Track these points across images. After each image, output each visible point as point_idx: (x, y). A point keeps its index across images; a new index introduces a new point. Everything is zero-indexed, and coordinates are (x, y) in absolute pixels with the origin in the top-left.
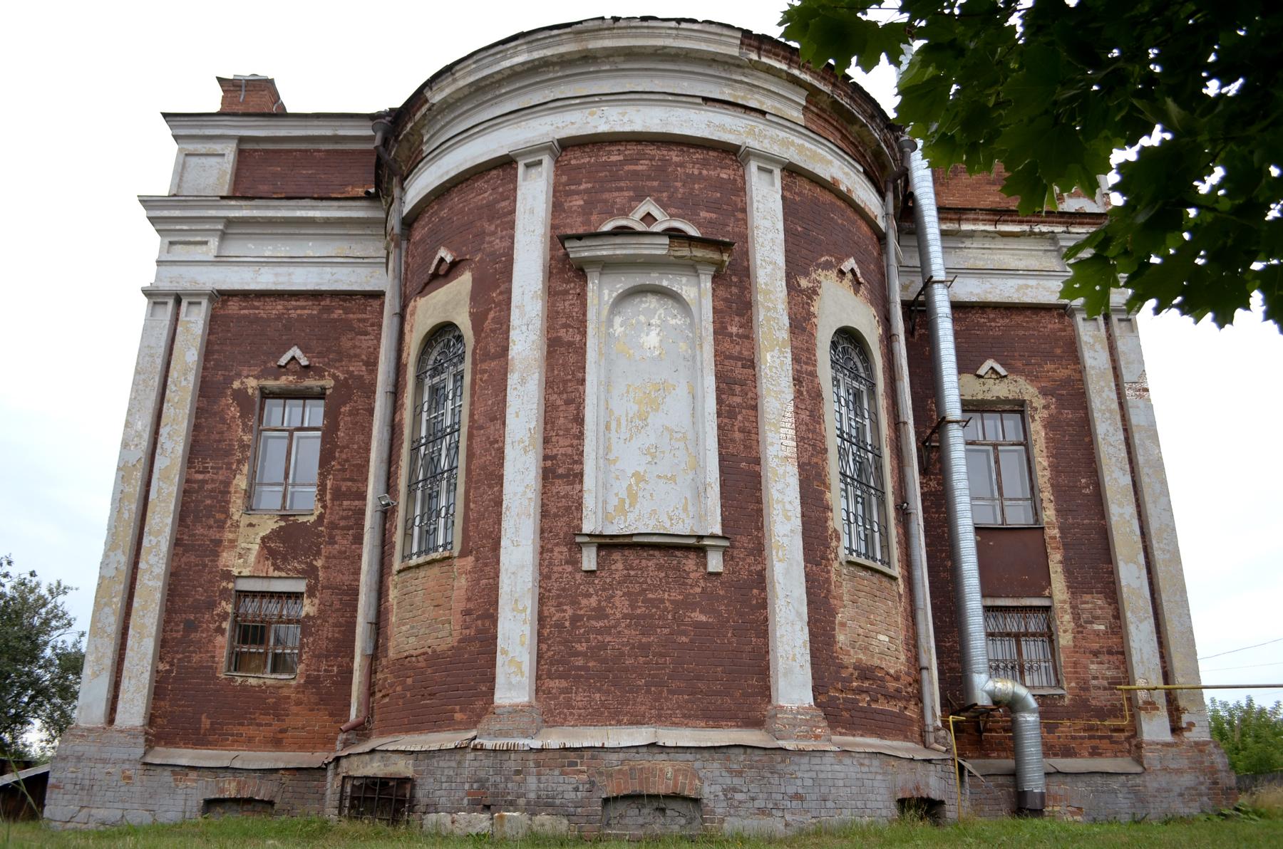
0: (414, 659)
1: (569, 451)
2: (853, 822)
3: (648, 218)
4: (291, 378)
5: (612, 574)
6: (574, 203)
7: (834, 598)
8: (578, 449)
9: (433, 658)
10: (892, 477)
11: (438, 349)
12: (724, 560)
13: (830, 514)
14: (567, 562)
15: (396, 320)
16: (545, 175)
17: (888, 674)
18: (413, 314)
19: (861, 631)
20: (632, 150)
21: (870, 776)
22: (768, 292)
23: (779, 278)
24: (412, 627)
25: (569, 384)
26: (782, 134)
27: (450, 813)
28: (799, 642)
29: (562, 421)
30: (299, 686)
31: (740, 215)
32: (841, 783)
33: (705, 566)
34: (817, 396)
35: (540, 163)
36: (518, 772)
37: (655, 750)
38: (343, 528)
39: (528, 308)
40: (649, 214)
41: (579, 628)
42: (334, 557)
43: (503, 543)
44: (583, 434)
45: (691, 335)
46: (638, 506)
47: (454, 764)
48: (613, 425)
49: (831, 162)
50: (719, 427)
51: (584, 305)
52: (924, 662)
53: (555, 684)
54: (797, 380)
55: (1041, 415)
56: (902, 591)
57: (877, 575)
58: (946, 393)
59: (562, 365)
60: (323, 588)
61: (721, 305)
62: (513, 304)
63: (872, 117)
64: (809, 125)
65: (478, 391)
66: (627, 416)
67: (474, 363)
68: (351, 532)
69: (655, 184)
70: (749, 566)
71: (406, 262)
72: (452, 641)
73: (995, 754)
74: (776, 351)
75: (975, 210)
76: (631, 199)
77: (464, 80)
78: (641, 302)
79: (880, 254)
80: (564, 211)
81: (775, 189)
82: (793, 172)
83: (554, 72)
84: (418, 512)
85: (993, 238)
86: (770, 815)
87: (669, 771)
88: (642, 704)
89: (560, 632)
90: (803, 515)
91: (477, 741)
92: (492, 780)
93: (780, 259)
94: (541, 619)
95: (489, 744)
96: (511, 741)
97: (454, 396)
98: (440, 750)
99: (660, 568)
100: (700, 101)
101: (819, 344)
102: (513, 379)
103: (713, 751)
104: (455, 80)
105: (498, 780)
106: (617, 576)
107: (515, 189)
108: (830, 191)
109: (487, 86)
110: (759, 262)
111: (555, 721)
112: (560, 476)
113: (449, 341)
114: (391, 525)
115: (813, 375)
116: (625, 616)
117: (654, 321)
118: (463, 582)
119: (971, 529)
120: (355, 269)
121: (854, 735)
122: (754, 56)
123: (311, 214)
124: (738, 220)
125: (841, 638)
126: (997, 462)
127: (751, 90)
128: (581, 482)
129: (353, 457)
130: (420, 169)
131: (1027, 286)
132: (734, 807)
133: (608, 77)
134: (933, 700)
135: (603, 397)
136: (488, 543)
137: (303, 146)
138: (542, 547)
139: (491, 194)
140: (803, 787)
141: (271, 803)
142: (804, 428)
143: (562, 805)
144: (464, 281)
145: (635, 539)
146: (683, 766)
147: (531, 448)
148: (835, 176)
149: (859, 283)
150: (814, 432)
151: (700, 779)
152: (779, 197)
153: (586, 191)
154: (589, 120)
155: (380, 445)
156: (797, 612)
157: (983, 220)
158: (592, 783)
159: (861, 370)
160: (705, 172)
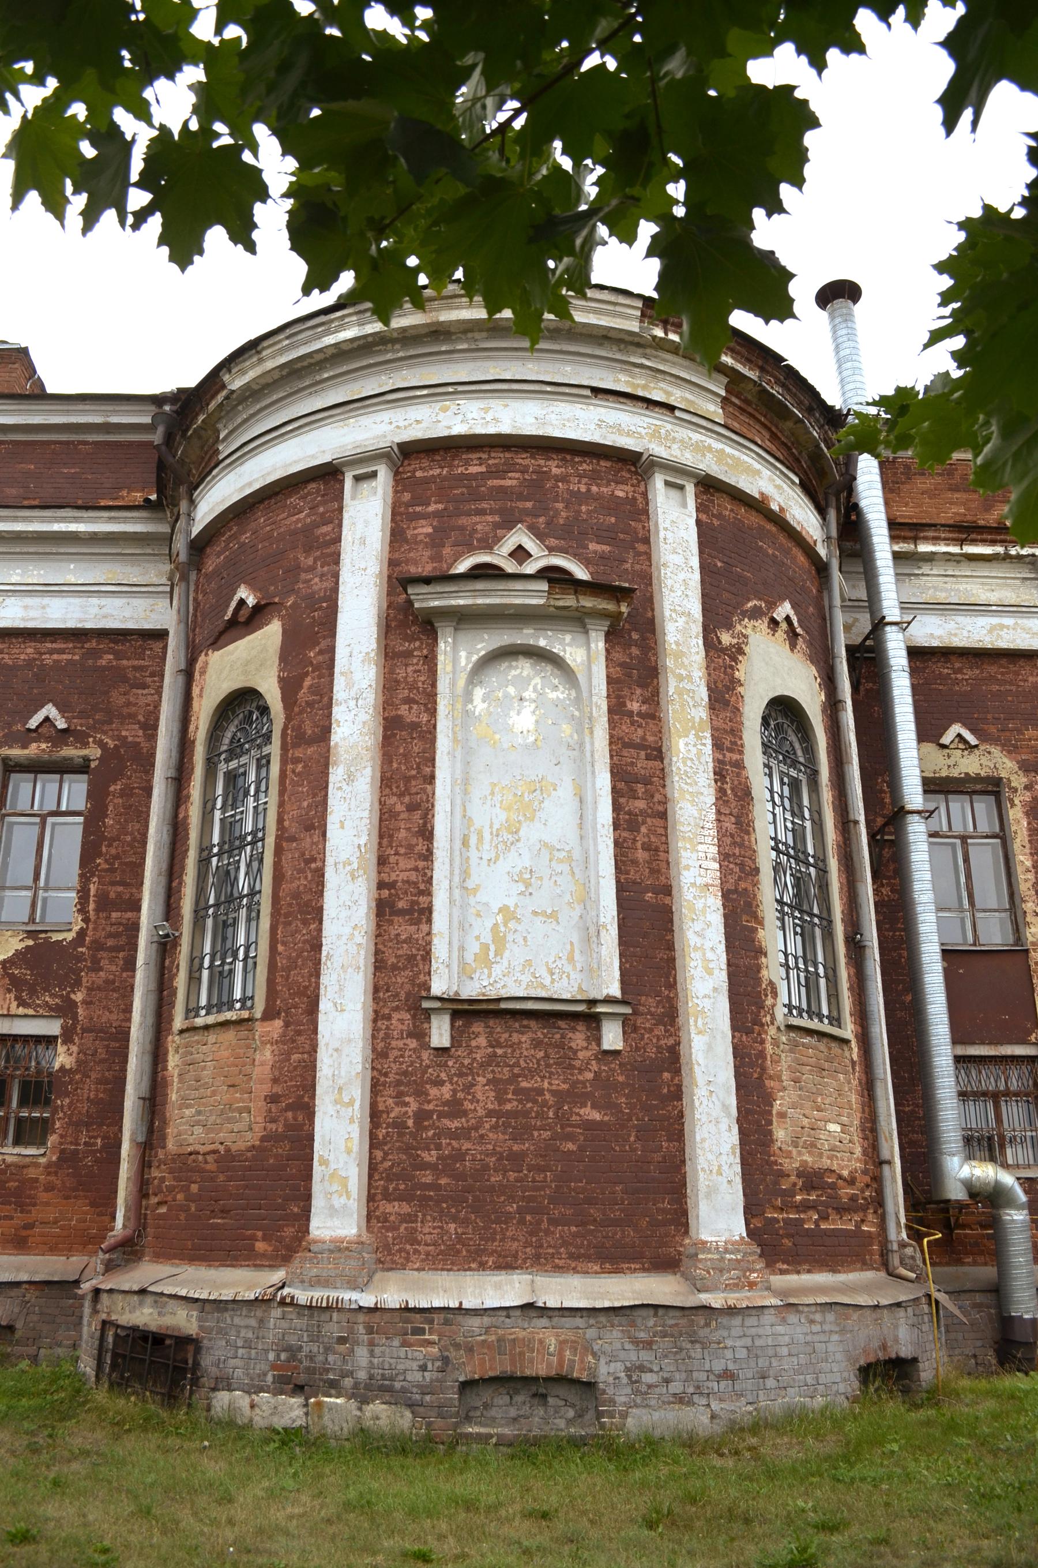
0: (200, 1158)
1: (413, 876)
2: (804, 1406)
3: (520, 554)
4: (44, 746)
5: (471, 1052)
6: (420, 530)
7: (771, 1078)
8: (425, 874)
9: (227, 1159)
10: (841, 899)
11: (236, 722)
12: (624, 1033)
13: (763, 960)
14: (410, 1035)
15: (181, 679)
16: (380, 491)
17: (840, 1177)
18: (203, 673)
19: (805, 1122)
20: (497, 458)
21: (823, 1337)
22: (678, 655)
23: (694, 633)
24: (199, 1113)
25: (413, 783)
26: (696, 437)
27: (249, 1393)
28: (726, 1148)
29: (403, 834)
30: (49, 1165)
31: (641, 547)
32: (784, 1351)
33: (598, 1041)
34: (745, 795)
35: (374, 475)
36: (342, 1340)
37: (533, 1313)
38: (112, 949)
39: (357, 676)
40: (520, 547)
41: (426, 1128)
42: (99, 989)
43: (322, 1006)
44: (431, 853)
45: (577, 713)
46: (507, 954)
47: (253, 1322)
48: (473, 840)
49: (758, 472)
50: (616, 843)
51: (433, 672)
52: (885, 1155)
53: (393, 1208)
54: (720, 775)
55: (1021, 798)
56: (855, 1057)
57: (825, 1040)
58: (904, 773)
59: (404, 755)
60: (84, 1030)
61: (617, 673)
62: (337, 670)
63: (810, 411)
64: (730, 422)
65: (289, 788)
66: (491, 827)
67: (284, 748)
68: (121, 955)
69: (529, 505)
70: (658, 1039)
71: (195, 599)
72: (252, 1138)
73: (970, 1260)
74: (691, 737)
75: (935, 525)
76: (497, 526)
77: (273, 361)
78: (510, 667)
79: (820, 591)
80: (407, 541)
81: (687, 512)
82: (710, 487)
83: (393, 351)
84: (207, 949)
85: (958, 562)
86: (690, 1403)
87: (552, 1343)
88: (513, 1239)
89: (401, 1135)
90: (729, 964)
91: (286, 1291)
92: (306, 1349)
93: (695, 607)
94: (375, 1114)
95: (302, 1296)
96: (334, 1294)
97: (257, 791)
98: (234, 1301)
99: (537, 1044)
100: (588, 392)
101: (746, 723)
102: (336, 775)
103: (611, 1313)
104: (261, 361)
105: (315, 1349)
106: (478, 1056)
107: (340, 509)
108: (758, 511)
109: (304, 368)
110: (667, 613)
111: (393, 1262)
112: (401, 912)
113: (251, 713)
114: (172, 962)
115: (739, 765)
116: (490, 1114)
117: (529, 694)
118: (267, 1055)
119: (938, 957)
120: (131, 600)
121: (798, 1272)
122: (659, 333)
123: (73, 527)
124: (639, 554)
125: (780, 1134)
126: (966, 860)
127: (655, 377)
128: (429, 921)
129: (124, 852)
130: (214, 477)
131: (1002, 627)
132: (641, 1393)
133: (466, 359)
134: (896, 1204)
135: (458, 801)
136: (303, 1004)
137: (64, 437)
138: (376, 1012)
139: (308, 515)
140: (735, 1360)
141: (10, 1328)
142: (728, 840)
143: (404, 1390)
144: (272, 633)
145: (503, 1005)
146: (570, 1336)
147: (361, 872)
148: (764, 490)
149: (796, 635)
150: (741, 845)
151: (594, 1354)
152: (692, 522)
153: (436, 514)
154: (440, 418)
155: (158, 848)
156: (724, 1105)
157: (945, 539)
158: (446, 1360)
159: (799, 753)
160: (594, 489)
